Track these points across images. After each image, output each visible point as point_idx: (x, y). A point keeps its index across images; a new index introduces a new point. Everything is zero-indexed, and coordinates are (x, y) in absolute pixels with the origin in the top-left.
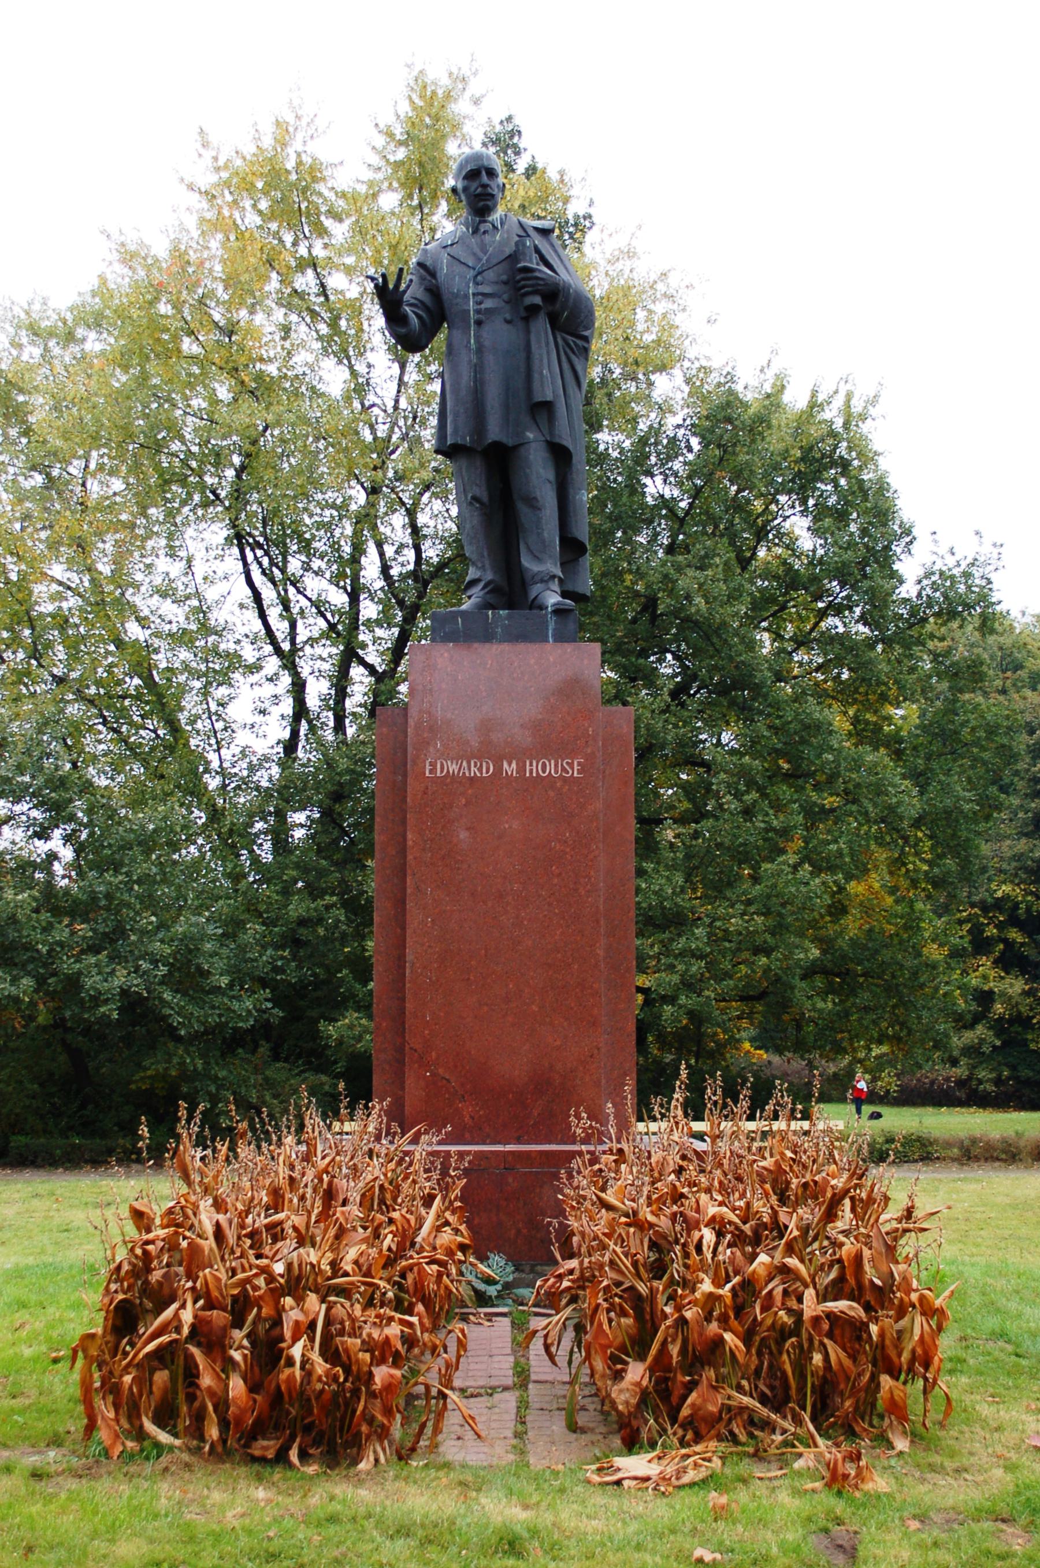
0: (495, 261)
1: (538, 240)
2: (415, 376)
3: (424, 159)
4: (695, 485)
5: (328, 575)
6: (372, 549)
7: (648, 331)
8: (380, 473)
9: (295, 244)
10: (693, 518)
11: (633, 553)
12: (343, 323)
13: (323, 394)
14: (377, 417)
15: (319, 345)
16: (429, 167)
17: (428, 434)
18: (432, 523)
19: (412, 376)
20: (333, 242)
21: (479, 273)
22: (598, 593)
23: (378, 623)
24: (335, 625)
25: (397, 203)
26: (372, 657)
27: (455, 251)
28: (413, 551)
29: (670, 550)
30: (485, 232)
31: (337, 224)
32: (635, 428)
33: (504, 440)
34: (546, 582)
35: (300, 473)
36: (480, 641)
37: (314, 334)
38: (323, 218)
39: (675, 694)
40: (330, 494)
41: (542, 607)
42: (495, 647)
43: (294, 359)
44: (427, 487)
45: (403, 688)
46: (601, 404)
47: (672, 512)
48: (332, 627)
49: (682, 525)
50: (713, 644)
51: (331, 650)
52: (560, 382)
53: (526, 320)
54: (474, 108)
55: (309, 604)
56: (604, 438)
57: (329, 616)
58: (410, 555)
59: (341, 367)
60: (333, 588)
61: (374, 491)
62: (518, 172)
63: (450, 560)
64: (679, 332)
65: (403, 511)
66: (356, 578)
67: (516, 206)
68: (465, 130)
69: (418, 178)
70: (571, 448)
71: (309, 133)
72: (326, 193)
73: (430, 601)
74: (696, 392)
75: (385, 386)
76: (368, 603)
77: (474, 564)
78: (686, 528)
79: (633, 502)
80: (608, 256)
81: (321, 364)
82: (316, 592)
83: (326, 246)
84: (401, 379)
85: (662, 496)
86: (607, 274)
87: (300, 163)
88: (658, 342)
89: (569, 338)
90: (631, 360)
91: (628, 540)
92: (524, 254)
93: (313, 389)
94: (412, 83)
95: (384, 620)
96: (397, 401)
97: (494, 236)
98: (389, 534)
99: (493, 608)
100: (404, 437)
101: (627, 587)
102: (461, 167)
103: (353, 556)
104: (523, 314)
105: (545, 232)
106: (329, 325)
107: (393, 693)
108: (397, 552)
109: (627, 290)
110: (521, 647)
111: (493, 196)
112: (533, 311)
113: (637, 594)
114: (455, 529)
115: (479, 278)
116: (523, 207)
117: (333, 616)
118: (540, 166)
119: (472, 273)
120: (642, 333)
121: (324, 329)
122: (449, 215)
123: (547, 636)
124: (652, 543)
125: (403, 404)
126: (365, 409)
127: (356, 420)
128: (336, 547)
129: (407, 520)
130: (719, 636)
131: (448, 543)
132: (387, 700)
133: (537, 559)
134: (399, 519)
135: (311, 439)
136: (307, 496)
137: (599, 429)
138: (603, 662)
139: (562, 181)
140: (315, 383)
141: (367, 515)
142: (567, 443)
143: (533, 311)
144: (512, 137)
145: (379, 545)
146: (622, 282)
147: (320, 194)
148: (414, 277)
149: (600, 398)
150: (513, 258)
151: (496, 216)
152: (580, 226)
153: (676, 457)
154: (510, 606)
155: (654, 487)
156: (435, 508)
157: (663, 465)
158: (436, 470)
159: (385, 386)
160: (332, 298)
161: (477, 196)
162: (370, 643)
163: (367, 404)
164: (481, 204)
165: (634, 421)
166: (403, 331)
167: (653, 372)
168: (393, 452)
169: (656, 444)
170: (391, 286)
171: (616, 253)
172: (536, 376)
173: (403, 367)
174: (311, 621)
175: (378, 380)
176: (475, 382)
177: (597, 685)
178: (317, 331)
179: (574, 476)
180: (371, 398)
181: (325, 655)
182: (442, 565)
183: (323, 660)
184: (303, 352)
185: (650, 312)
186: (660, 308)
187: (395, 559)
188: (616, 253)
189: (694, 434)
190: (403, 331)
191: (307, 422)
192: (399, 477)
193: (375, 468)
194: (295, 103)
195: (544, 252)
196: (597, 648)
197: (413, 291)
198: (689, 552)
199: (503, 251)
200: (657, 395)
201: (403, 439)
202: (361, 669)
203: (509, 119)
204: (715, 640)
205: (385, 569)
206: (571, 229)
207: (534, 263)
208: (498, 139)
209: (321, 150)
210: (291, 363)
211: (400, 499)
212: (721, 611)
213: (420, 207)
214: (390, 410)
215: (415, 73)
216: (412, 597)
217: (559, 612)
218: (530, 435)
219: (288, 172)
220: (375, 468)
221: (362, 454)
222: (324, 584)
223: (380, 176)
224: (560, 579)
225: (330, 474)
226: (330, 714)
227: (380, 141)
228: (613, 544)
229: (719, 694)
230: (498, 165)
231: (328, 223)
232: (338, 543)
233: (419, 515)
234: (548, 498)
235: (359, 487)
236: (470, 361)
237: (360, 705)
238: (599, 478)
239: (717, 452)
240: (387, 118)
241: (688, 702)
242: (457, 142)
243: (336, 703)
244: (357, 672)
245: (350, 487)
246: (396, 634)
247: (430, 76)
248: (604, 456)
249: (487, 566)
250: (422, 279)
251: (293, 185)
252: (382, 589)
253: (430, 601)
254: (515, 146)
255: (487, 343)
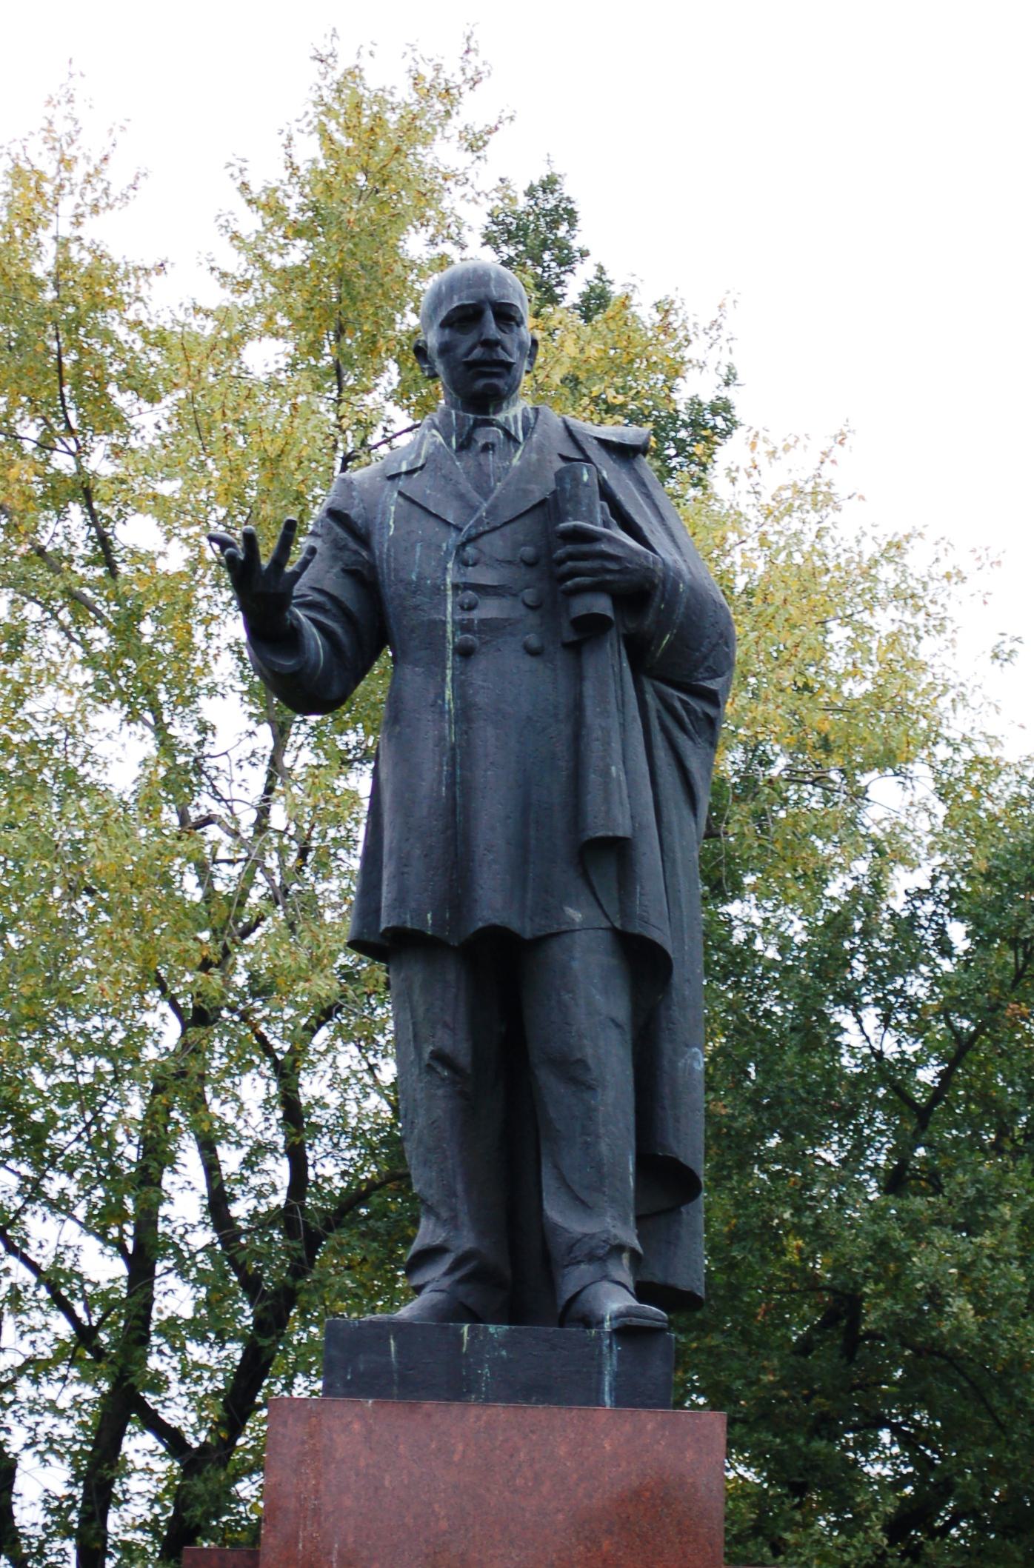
0: (508, 514)
1: (609, 470)
2: (307, 756)
3: (352, 265)
4: (957, 1033)
5: (81, 1212)
6: (189, 1155)
7: (854, 673)
8: (216, 977)
9: (45, 445)
10: (950, 1109)
11: (807, 1187)
12: (147, 627)
13: (92, 788)
14: (216, 845)
15: (88, 675)
16: (360, 284)
17: (335, 890)
18: (333, 1098)
19: (301, 757)
20: (134, 443)
21: (470, 540)
22: (720, 1279)
23: (197, 1330)
24: (93, 1331)
25: (283, 361)
26: (177, 1413)
27: (420, 487)
28: (285, 1162)
29: (895, 1182)
30: (486, 448)
31: (146, 407)
32: (818, 892)
33: (515, 925)
34: (602, 1260)
35: (33, 967)
36: (437, 1397)
37: (78, 651)
38: (112, 389)
39: (896, 1528)
40: (96, 1021)
41: (590, 1321)
42: (473, 1412)
43: (30, 706)
44: (326, 1014)
45: (246, 1488)
46: (741, 836)
47: (900, 1091)
48: (85, 1335)
49: (923, 1125)
50: (991, 1412)
51: (76, 1392)
52: (645, 768)
53: (575, 649)
54: (470, 156)
55: (31, 1278)
56: (742, 910)
57: (79, 1308)
58: (280, 1171)
59: (138, 728)
60: (92, 1244)
61: (199, 1017)
62: (566, 303)
63: (373, 1186)
64: (927, 678)
65: (266, 1067)
66: (147, 1220)
67: (556, 379)
68: (446, 204)
69: (335, 301)
70: (669, 947)
71: (89, 197)
72: (122, 333)
73: (320, 1283)
74: (965, 821)
75: (238, 775)
76: (173, 1281)
77: (431, 1210)
78: (934, 1133)
79: (810, 1067)
80: (766, 499)
81: (93, 721)
82: (50, 1251)
83: (117, 452)
84: (275, 761)
85: (879, 1055)
86: (763, 541)
87: (64, 264)
88: (877, 699)
89: (675, 695)
90: (813, 738)
91: (796, 1158)
92: (575, 499)
93: (69, 777)
94: (329, 96)
95: (209, 1325)
96: (263, 812)
97: (509, 457)
98: (230, 1119)
99: (474, 1317)
100: (278, 896)
101: (790, 1267)
102: (439, 298)
103: (142, 1168)
104: (569, 636)
105: (625, 453)
106: (113, 632)
107: (223, 1499)
108: (248, 1163)
109: (807, 579)
110: (538, 1414)
111: (508, 366)
112: (592, 628)
113: (813, 1284)
114: (387, 1113)
115: (470, 550)
116: (572, 382)
117: (88, 1309)
118: (616, 290)
119: (453, 539)
120: (840, 679)
121: (100, 638)
122: (400, 396)
123: (599, 1391)
124: (848, 1166)
125: (278, 818)
126: (192, 827)
127: (166, 853)
128: (102, 1143)
129: (274, 1088)
130: (1007, 1393)
131: (368, 1145)
132: (208, 1516)
133: (582, 1205)
134: (255, 1087)
135: (58, 892)
136: (42, 1025)
137: (737, 891)
138: (730, 1444)
139: (666, 328)
140: (74, 762)
141: (182, 1074)
142: (661, 935)
143: (592, 628)
144: (553, 225)
145: (207, 1147)
146: (798, 559)
147: (108, 337)
148: (317, 543)
149: (738, 820)
150: (550, 508)
151: (514, 412)
152: (709, 425)
153: (913, 965)
154: (515, 1313)
155: (861, 1033)
156: (343, 1061)
157: (882, 982)
158: (348, 975)
159: (238, 775)
160: (123, 569)
161: (470, 365)
162: (173, 1377)
163: (194, 814)
164: (481, 383)
165: (818, 878)
166: (289, 663)
167: (864, 769)
168: (247, 932)
169: (866, 933)
170: (265, 563)
171: (787, 494)
172: (593, 778)
173: (281, 734)
174: (36, 1318)
175: (222, 762)
176: (451, 786)
177: (719, 1508)
178: (86, 645)
179: (676, 1012)
180: (205, 803)
181: (63, 1403)
182: (351, 1200)
183: (60, 1413)
184: (50, 690)
185: (862, 629)
186: (884, 620)
187: (242, 1180)
188: (787, 494)
189: (958, 915)
190: (289, 663)
191: (52, 851)
192: (261, 988)
193: (205, 966)
194: (62, 128)
195: (621, 497)
196: (716, 1423)
197: (315, 572)
198: (938, 1190)
199: (526, 492)
200: (874, 817)
201: (273, 900)
202: (148, 1440)
203: (549, 184)
204: (996, 1401)
205: (218, 1203)
206: (683, 434)
207: (596, 520)
208: (523, 228)
209: (118, 237)
210: (21, 714)
211: (261, 1038)
212: (1013, 1332)
213: (338, 372)
214: (247, 833)
215: (337, 75)
216: (273, 1270)
217: (628, 1332)
218: (576, 915)
219: (37, 284)
220: (205, 966)
221: (178, 932)
222: (71, 1232)
223: (248, 299)
224: (635, 1256)
225: (99, 974)
226: (70, 1546)
227: (250, 223)
228: (762, 1161)
229: (1004, 1533)
230: (524, 300)
231: (123, 400)
232: (109, 1135)
233: (304, 1078)
234: (612, 1061)
235: (165, 1007)
236: (442, 738)
237: (141, 1527)
238: (731, 1008)
239: (1010, 957)
240: (267, 172)
241: (930, 1548)
242: (425, 234)
243: (86, 1518)
244: (139, 1446)
245: (144, 1007)
246: (239, 1355)
247: (374, 80)
248: (742, 958)
249: (464, 1218)
250: (338, 546)
251: (46, 315)
252: (208, 1249)
253: (320, 1283)
254: (561, 245)
255: (481, 699)
